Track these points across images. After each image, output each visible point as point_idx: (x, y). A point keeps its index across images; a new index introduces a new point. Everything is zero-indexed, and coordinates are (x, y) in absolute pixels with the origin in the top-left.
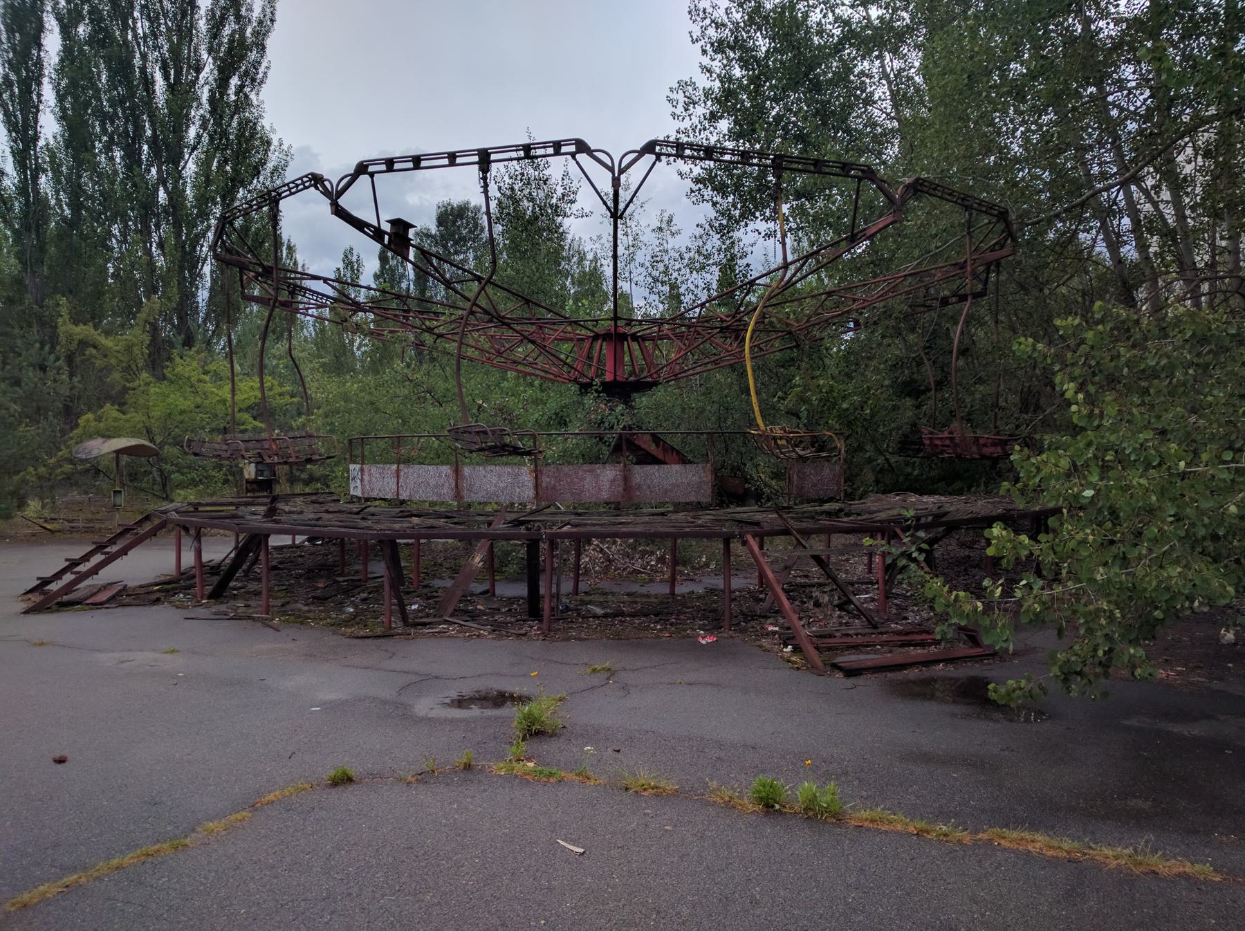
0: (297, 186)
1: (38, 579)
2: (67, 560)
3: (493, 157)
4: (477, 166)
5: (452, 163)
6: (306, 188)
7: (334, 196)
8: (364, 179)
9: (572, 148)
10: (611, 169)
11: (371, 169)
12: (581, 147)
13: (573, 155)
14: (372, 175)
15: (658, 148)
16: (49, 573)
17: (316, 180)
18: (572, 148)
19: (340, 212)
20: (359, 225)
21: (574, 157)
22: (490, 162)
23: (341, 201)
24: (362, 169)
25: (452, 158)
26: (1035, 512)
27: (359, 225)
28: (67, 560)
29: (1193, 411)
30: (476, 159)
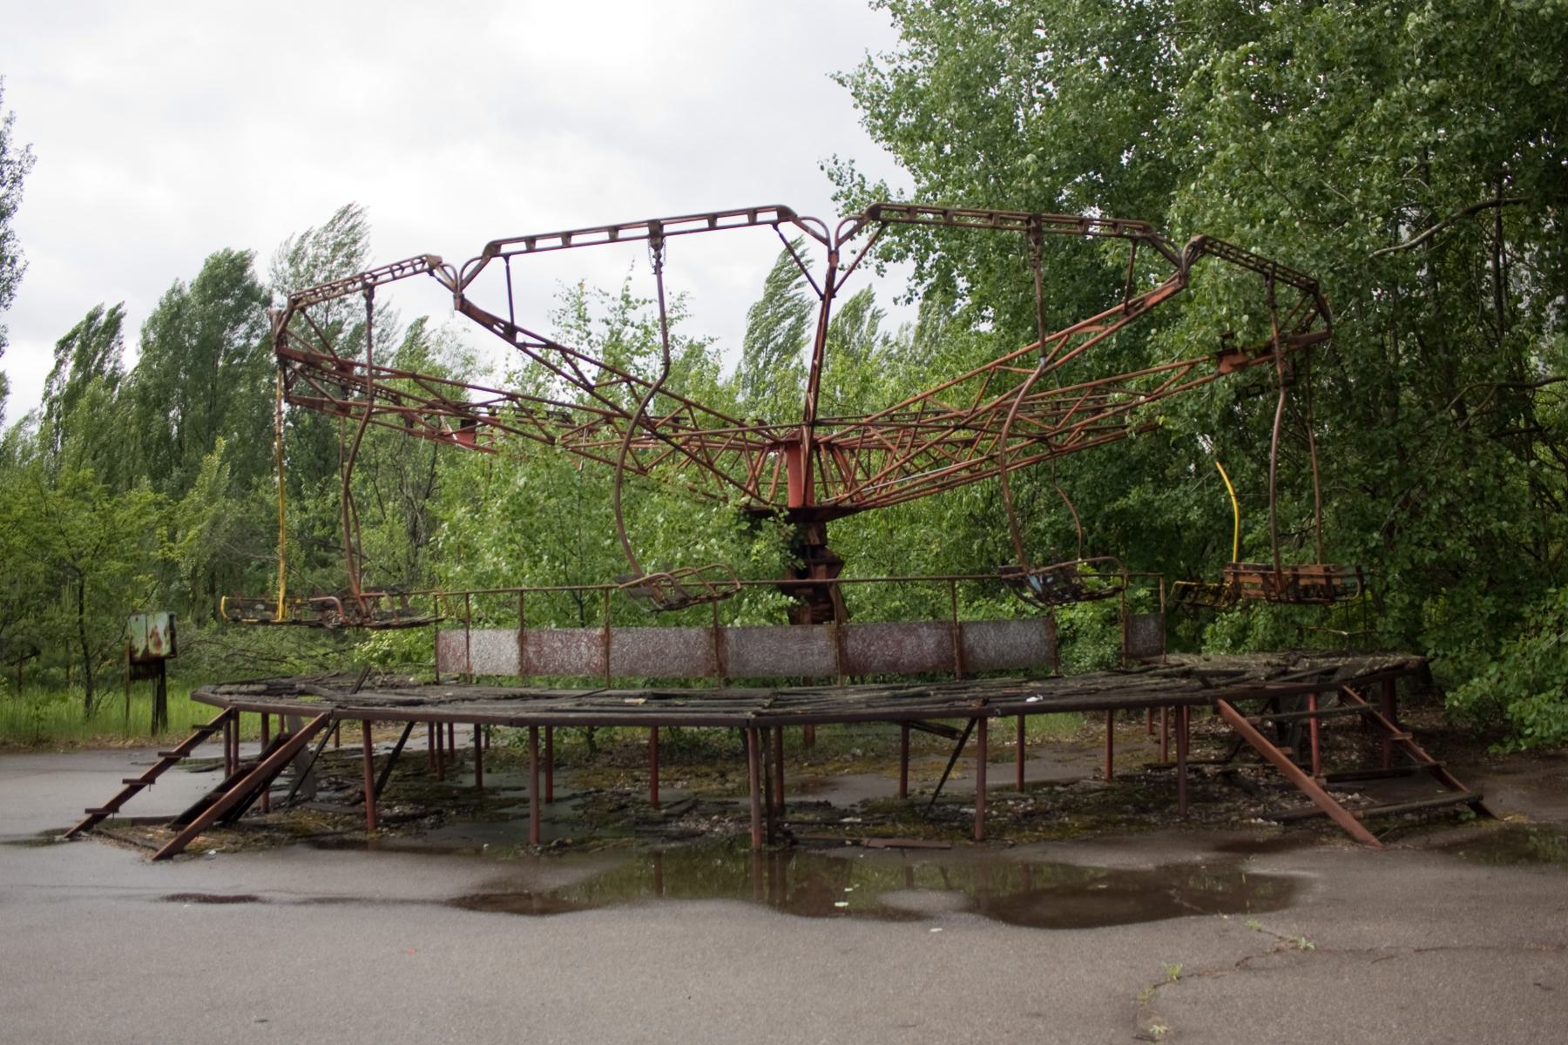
0: (403, 269)
1: (88, 811)
2: (125, 782)
3: (667, 229)
4: (646, 241)
5: (567, 244)
6: (416, 272)
7: (457, 287)
8: (497, 263)
9: (773, 216)
10: (826, 242)
11: (505, 249)
12: (785, 214)
13: (775, 225)
14: (507, 257)
15: (883, 214)
16: (101, 803)
17: (432, 265)
18: (773, 216)
19: (465, 307)
20: (487, 321)
21: (775, 227)
22: (663, 236)
23: (469, 293)
24: (493, 250)
25: (752, 213)
26: (1361, 676)
27: (487, 321)
28: (125, 782)
29: (1121, 455)
30: (645, 231)
